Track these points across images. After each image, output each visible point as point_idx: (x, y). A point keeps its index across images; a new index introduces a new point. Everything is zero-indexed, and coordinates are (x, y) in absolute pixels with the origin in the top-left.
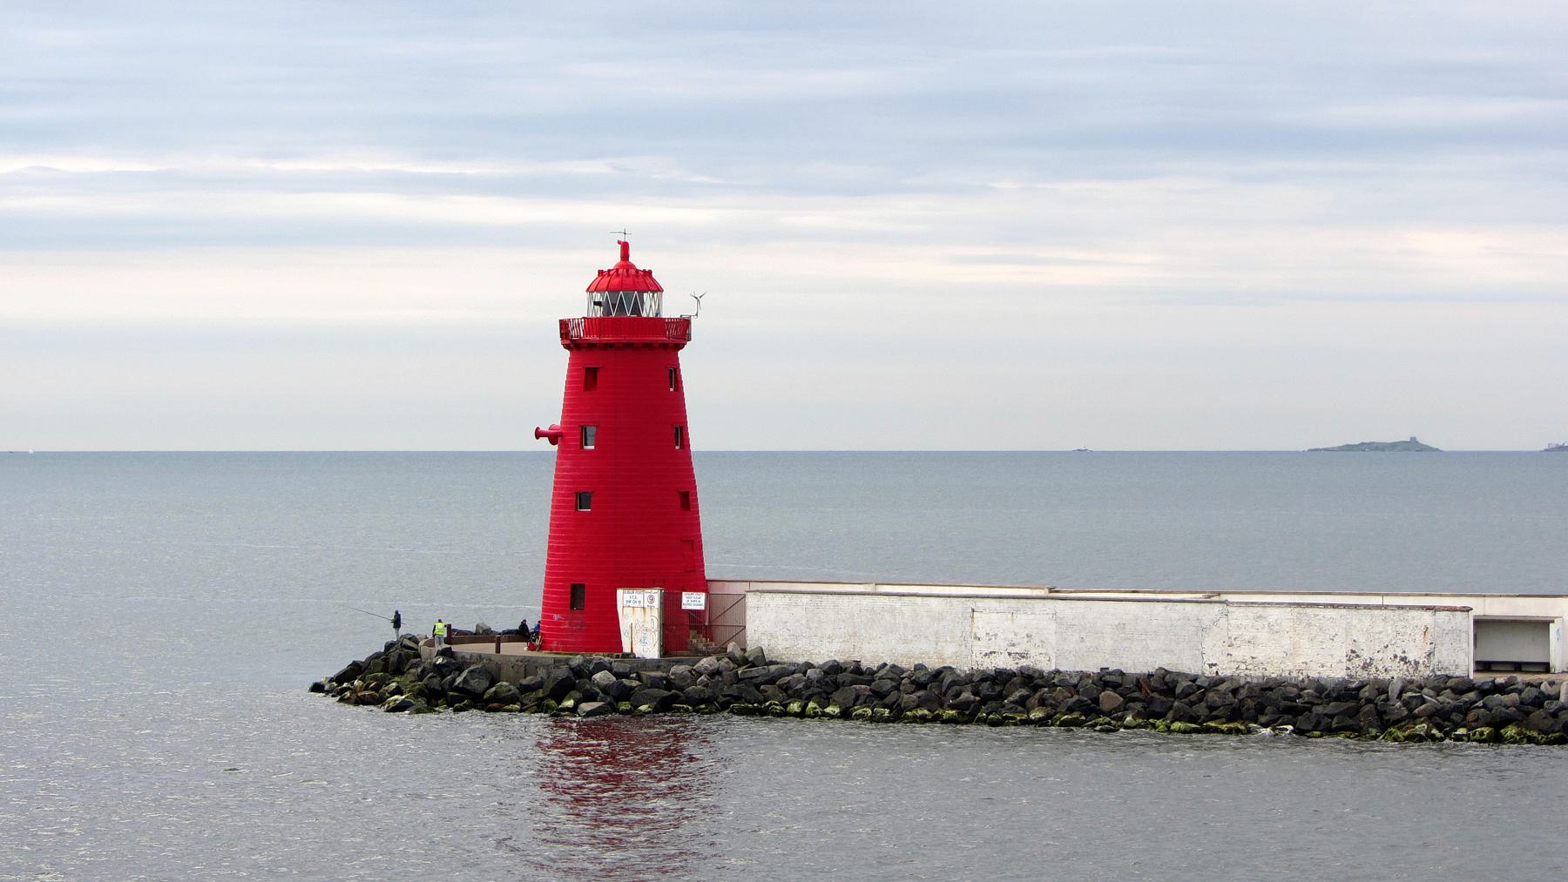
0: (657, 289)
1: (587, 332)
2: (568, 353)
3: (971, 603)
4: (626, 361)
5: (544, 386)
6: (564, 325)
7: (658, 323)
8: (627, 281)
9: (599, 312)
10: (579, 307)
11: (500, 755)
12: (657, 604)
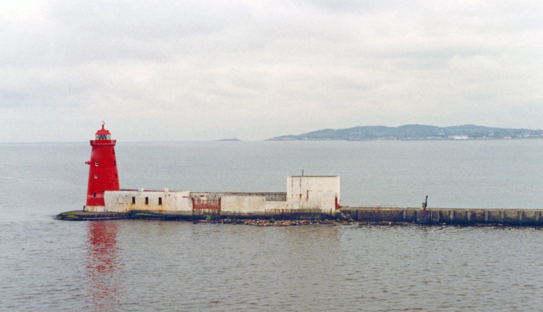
0: (109, 134)
5: (88, 154)
7: (109, 141)
8: (103, 133)
9: (98, 139)
10: (94, 138)
11: (82, 229)
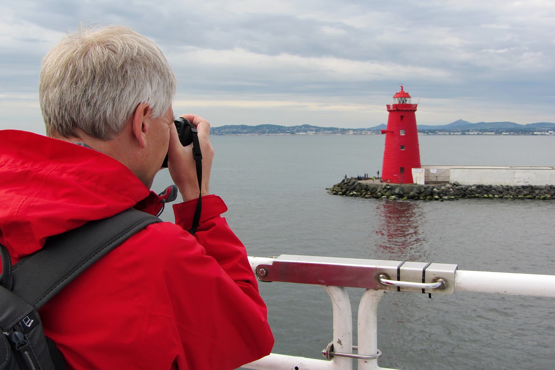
0: (409, 97)
1: (394, 107)
2: (388, 113)
3: (514, 171)
4: (403, 115)
6: (388, 106)
7: (410, 105)
12: (424, 172)
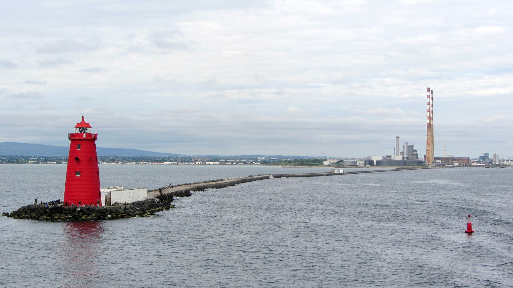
8: (83, 126)
11: (56, 231)
